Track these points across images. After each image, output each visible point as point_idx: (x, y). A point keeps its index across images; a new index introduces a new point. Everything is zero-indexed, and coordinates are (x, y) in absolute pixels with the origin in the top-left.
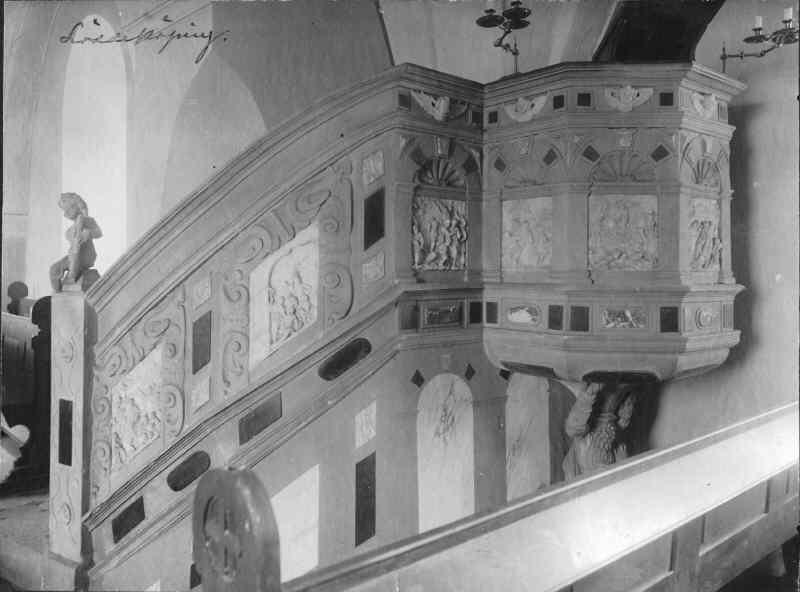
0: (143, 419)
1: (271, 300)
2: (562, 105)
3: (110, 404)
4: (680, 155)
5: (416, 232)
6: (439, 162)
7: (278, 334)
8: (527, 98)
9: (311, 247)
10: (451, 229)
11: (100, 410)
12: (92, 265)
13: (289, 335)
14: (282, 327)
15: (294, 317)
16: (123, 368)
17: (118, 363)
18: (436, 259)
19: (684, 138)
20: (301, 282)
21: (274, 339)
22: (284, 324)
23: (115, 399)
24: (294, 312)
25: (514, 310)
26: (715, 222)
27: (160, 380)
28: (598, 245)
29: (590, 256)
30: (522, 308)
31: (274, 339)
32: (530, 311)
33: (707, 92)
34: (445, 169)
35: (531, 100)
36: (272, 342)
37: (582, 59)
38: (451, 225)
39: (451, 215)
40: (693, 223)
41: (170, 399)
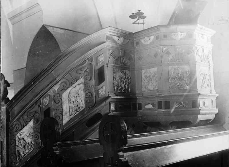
0: (27, 145)
1: (70, 102)
2: (159, 39)
3: (15, 140)
4: (196, 53)
5: (115, 80)
6: (121, 58)
7: (72, 113)
8: (147, 37)
9: (82, 85)
10: (125, 80)
11: (12, 143)
12: (7, 96)
13: (76, 113)
14: (73, 111)
15: (77, 107)
16: (19, 129)
17: (18, 127)
18: (121, 89)
19: (196, 48)
20: (79, 96)
21: (71, 114)
22: (74, 110)
23: (17, 139)
24: (77, 106)
25: (147, 104)
26: (208, 75)
27: (33, 131)
28: (172, 82)
29: (170, 85)
30: (149, 104)
31: (71, 114)
32: (151, 104)
33: (203, 34)
34: (123, 60)
35: (149, 37)
36: (70, 116)
37: (12, 82)
38: (125, 78)
39: (125, 75)
40: (201, 75)
41: (37, 137)
